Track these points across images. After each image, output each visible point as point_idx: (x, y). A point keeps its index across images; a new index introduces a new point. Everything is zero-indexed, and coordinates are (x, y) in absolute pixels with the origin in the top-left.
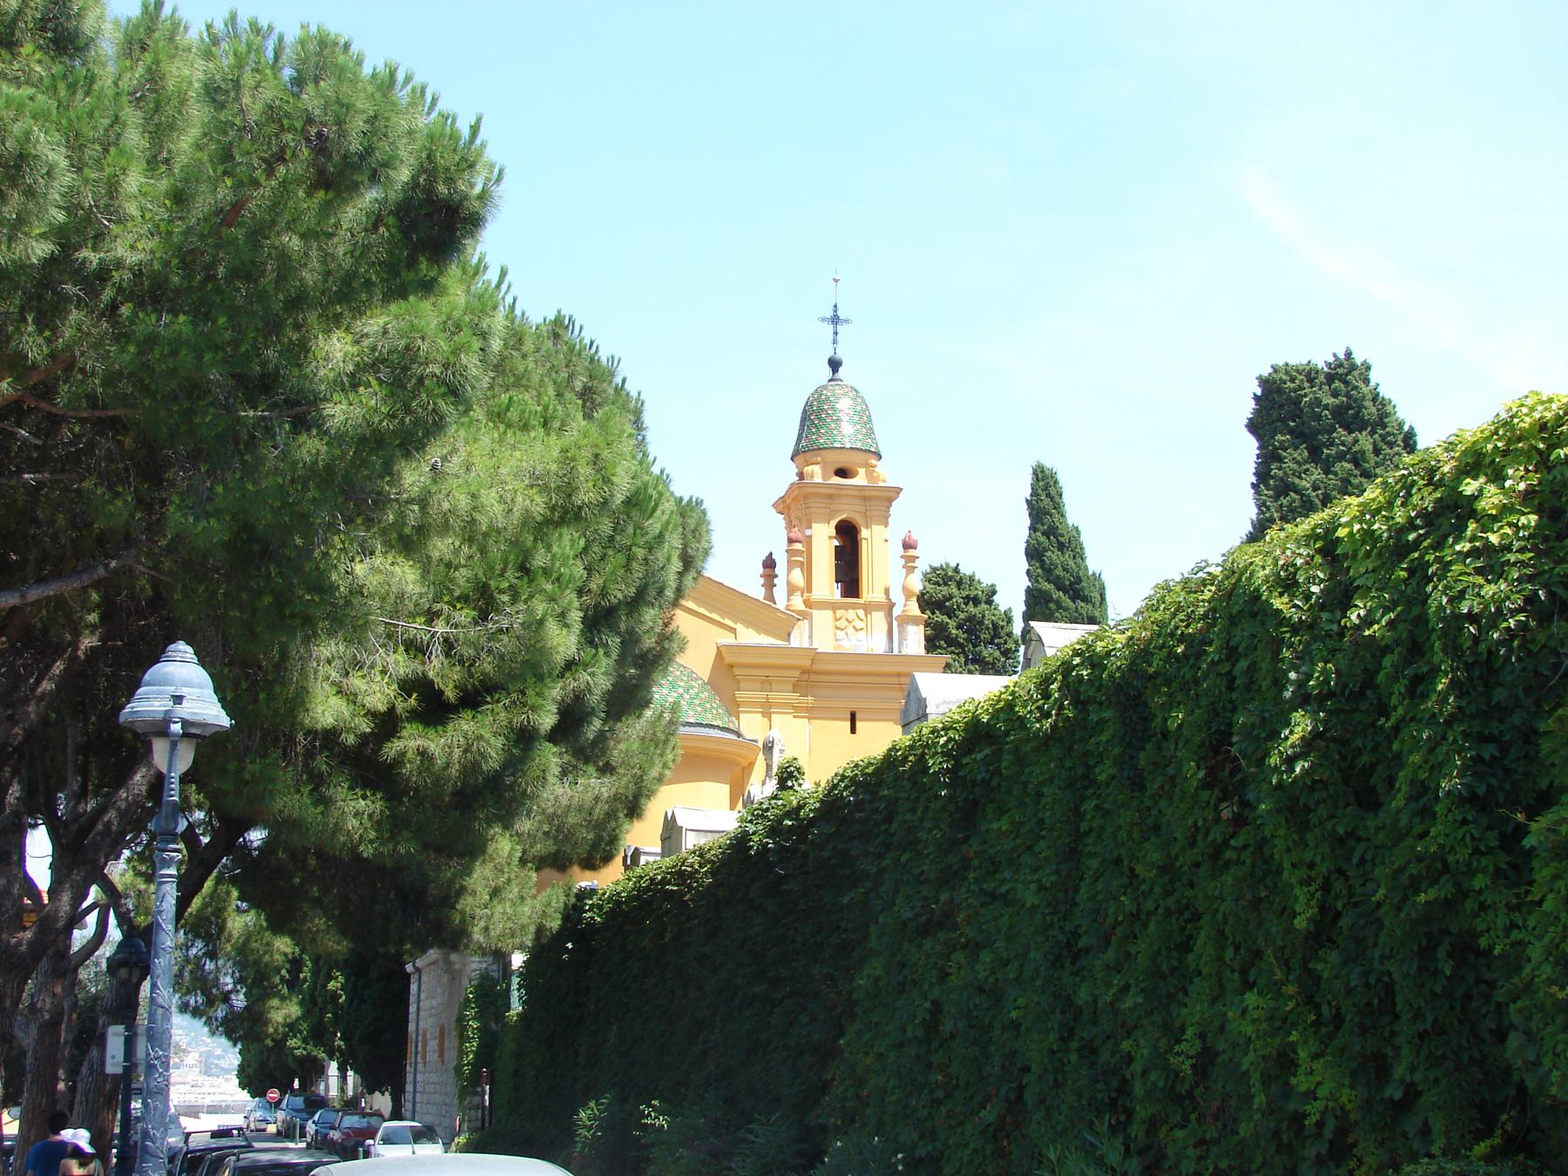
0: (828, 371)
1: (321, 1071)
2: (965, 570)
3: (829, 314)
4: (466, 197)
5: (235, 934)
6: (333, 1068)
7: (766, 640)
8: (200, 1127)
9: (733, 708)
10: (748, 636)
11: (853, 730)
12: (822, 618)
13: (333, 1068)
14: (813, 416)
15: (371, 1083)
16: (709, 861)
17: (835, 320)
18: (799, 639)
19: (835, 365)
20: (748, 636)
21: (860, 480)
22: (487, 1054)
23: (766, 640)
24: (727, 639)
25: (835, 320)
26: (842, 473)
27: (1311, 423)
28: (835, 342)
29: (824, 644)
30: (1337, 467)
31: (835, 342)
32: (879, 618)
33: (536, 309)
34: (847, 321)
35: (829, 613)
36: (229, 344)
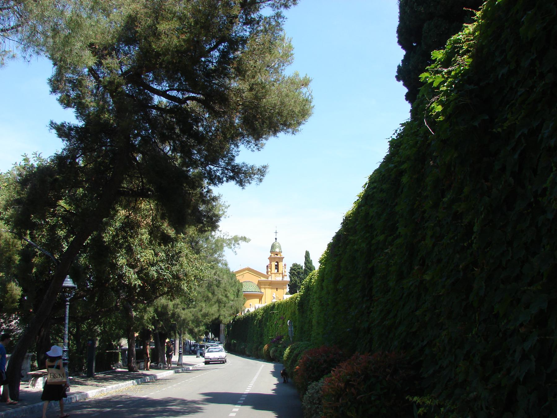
1: (208, 334)
2: (298, 264)
4: (176, 46)
6: (210, 333)
7: (265, 279)
8: (71, 388)
9: (260, 288)
10: (263, 279)
12: (273, 275)
13: (210, 333)
14: (273, 247)
15: (215, 336)
18: (270, 279)
19: (276, 239)
20: (263, 279)
21: (279, 256)
22: (228, 334)
23: (265, 279)
24: (260, 279)
26: (277, 255)
29: (273, 279)
32: (281, 275)
33: (275, 380)
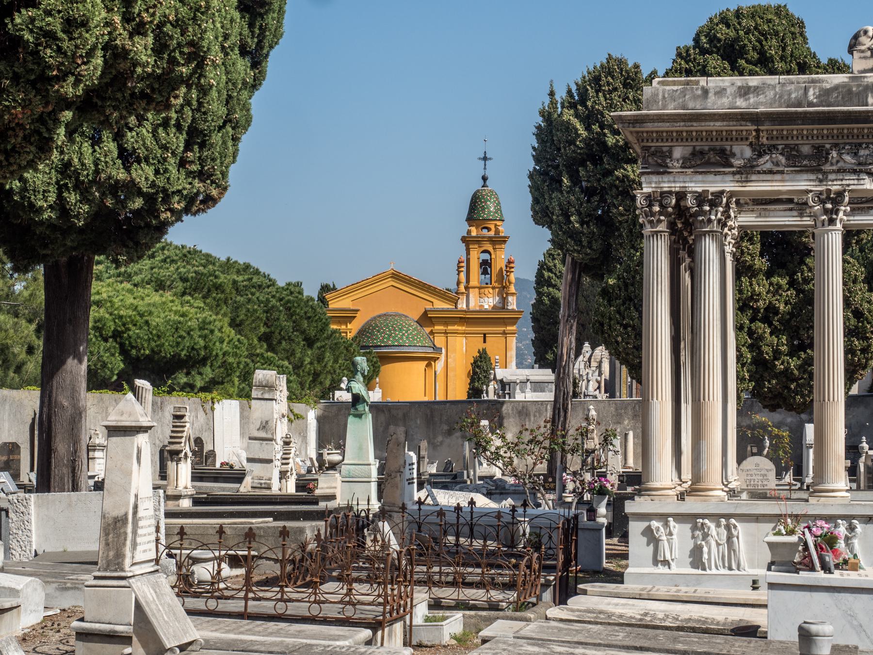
0: (481, 182)
3: (482, 156)
5: (169, 463)
10: (440, 305)
11: (485, 342)
14: (476, 204)
16: (279, 586)
17: (485, 159)
18: (462, 305)
20: (440, 305)
25: (485, 159)
27: (182, 221)
28: (485, 168)
30: (32, 139)
31: (485, 168)
34: (490, 159)
35: (477, 290)
36: (606, 212)
